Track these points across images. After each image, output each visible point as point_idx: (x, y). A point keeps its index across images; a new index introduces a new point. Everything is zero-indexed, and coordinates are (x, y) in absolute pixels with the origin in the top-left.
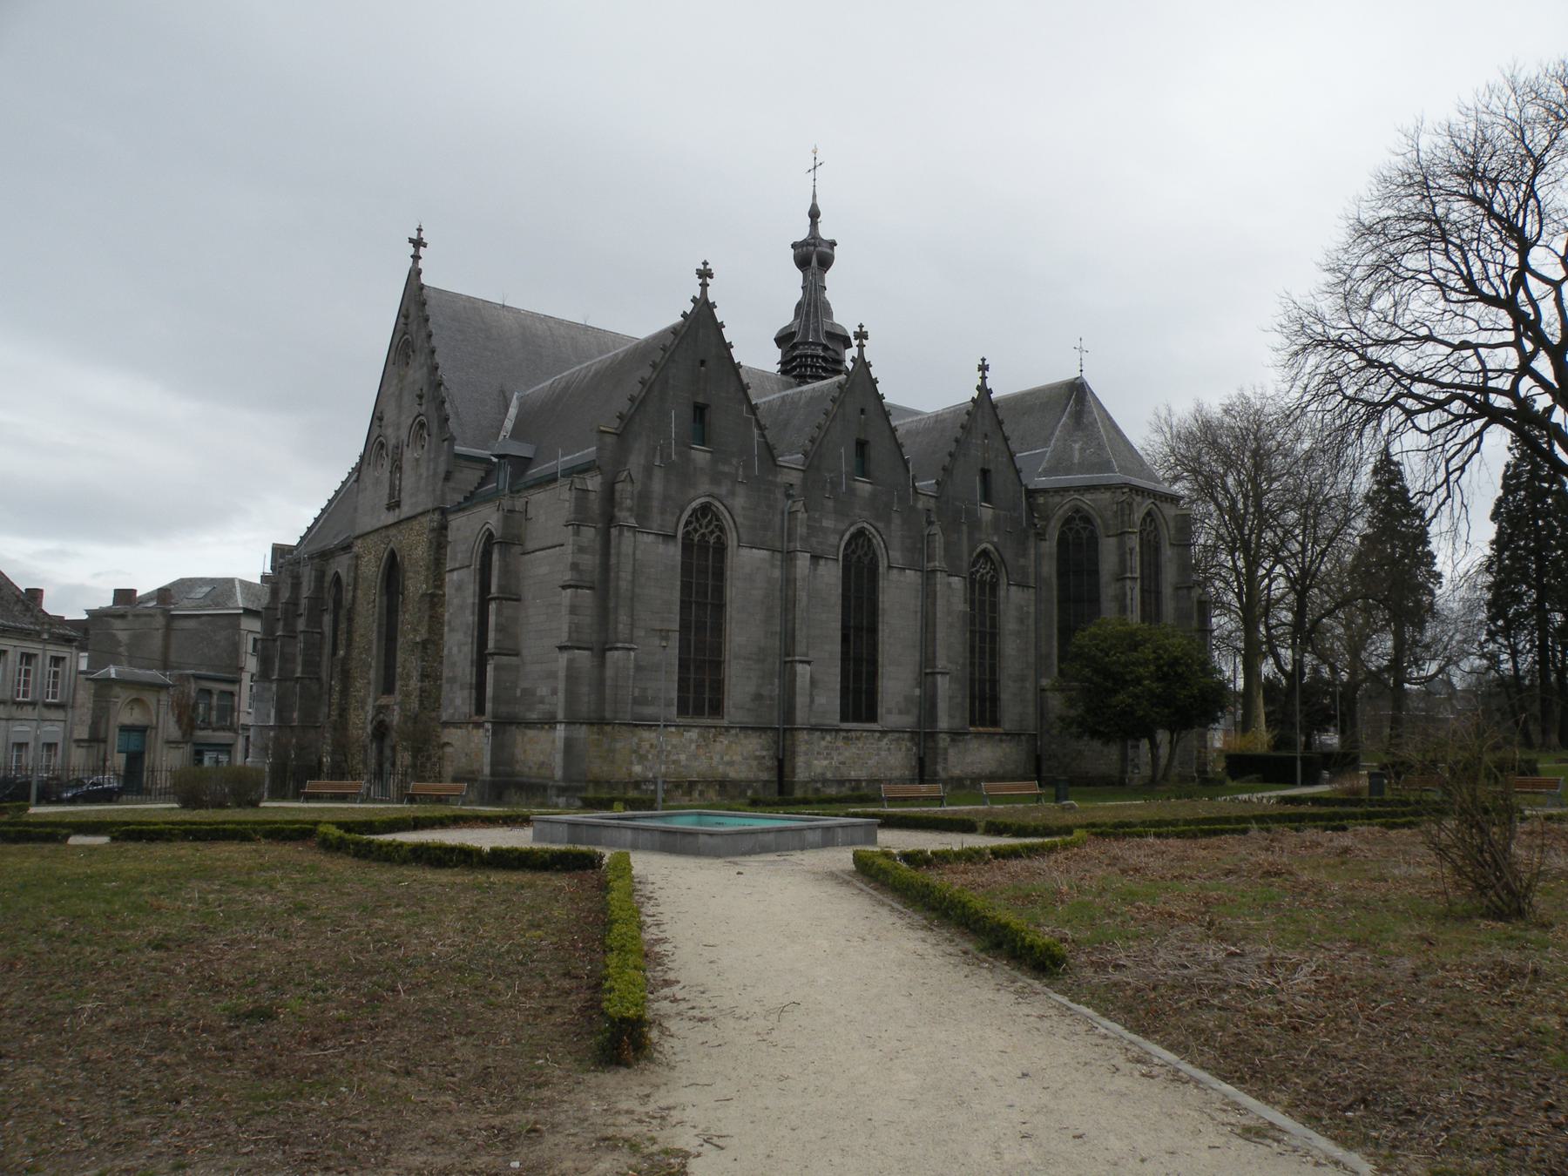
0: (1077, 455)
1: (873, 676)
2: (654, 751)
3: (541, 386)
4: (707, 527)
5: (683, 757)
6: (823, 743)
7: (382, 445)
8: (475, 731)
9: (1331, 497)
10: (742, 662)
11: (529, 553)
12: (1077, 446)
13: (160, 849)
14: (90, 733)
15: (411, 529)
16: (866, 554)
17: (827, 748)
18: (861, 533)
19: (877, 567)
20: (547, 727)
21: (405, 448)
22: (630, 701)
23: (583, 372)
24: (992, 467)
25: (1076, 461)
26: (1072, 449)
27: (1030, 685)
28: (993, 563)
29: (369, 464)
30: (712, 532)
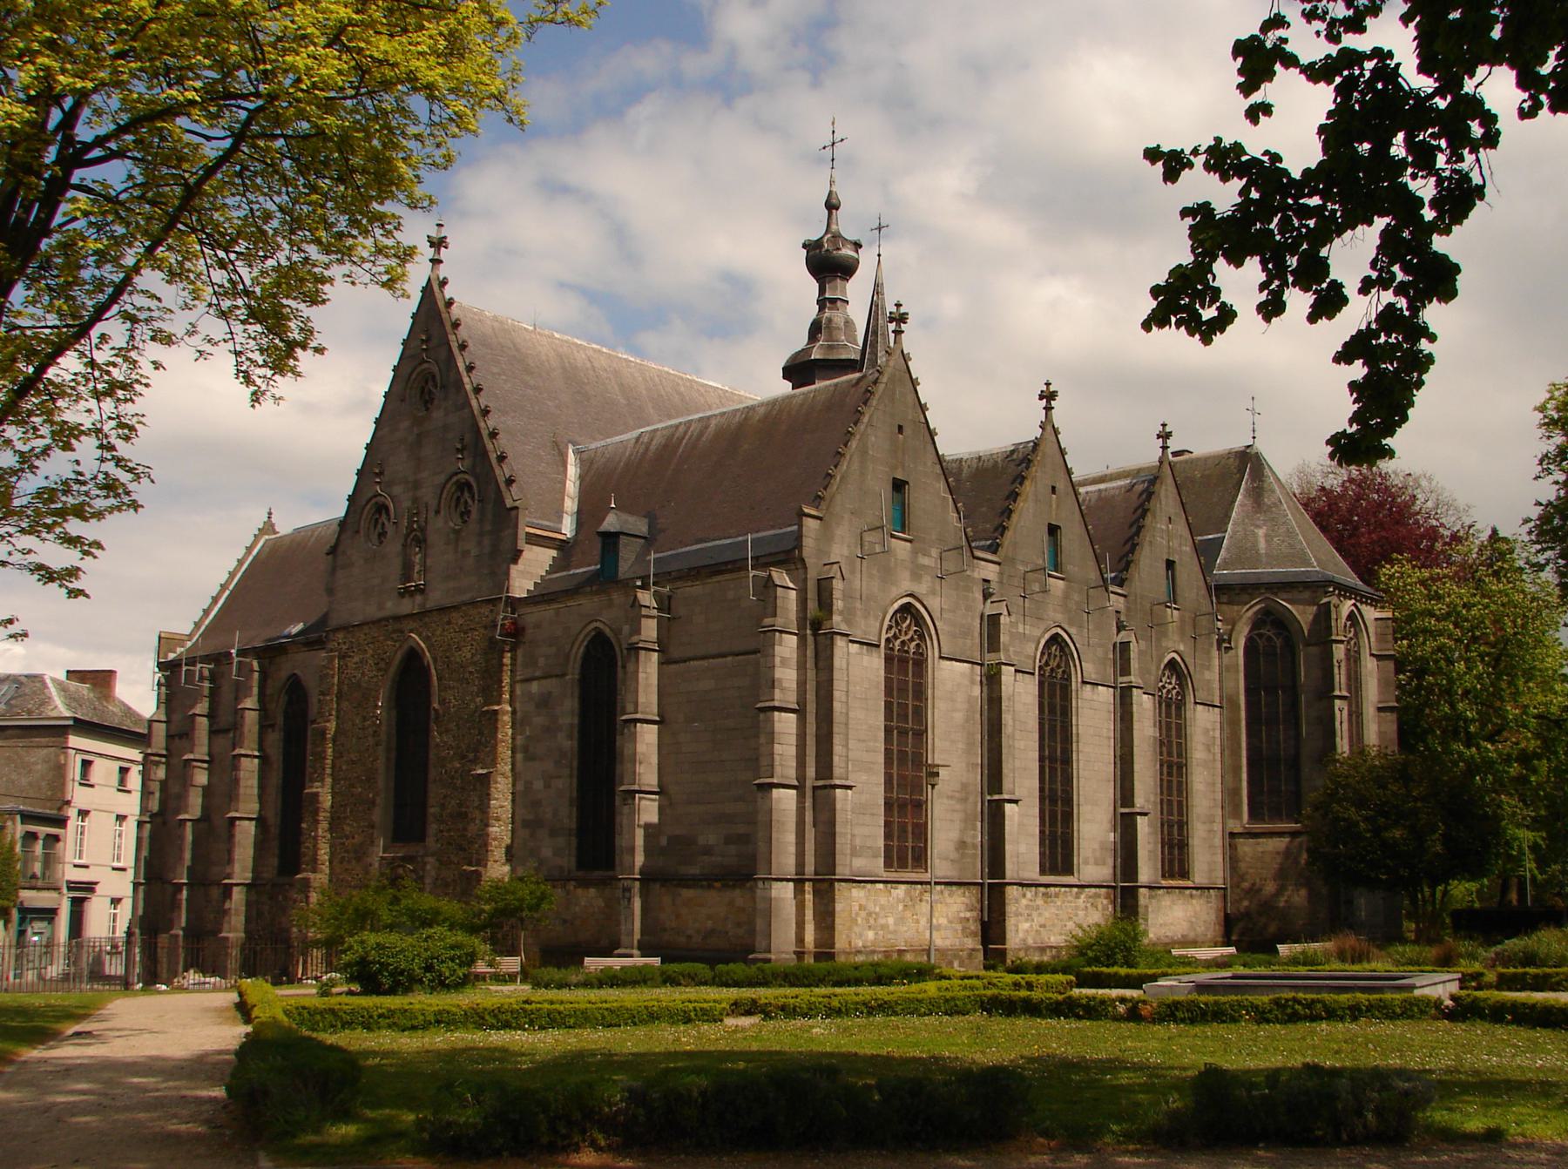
0: (1262, 545)
1: (1068, 817)
2: (863, 914)
3: (617, 439)
4: (906, 634)
5: (891, 921)
6: (1024, 902)
7: (382, 509)
8: (579, 891)
9: (462, 493)
10: (945, 801)
11: (676, 662)
12: (1261, 532)
13: (1022, 1023)
14: (1004, 893)
15: (449, 623)
16: (1059, 666)
17: (1027, 907)
18: (1055, 639)
19: (1069, 679)
20: (717, 885)
21: (432, 514)
22: (849, 851)
23: (682, 429)
24: (1175, 558)
25: (1263, 551)
26: (1255, 535)
27: (1218, 827)
28: (1178, 678)
29: (357, 532)
30: (912, 639)
